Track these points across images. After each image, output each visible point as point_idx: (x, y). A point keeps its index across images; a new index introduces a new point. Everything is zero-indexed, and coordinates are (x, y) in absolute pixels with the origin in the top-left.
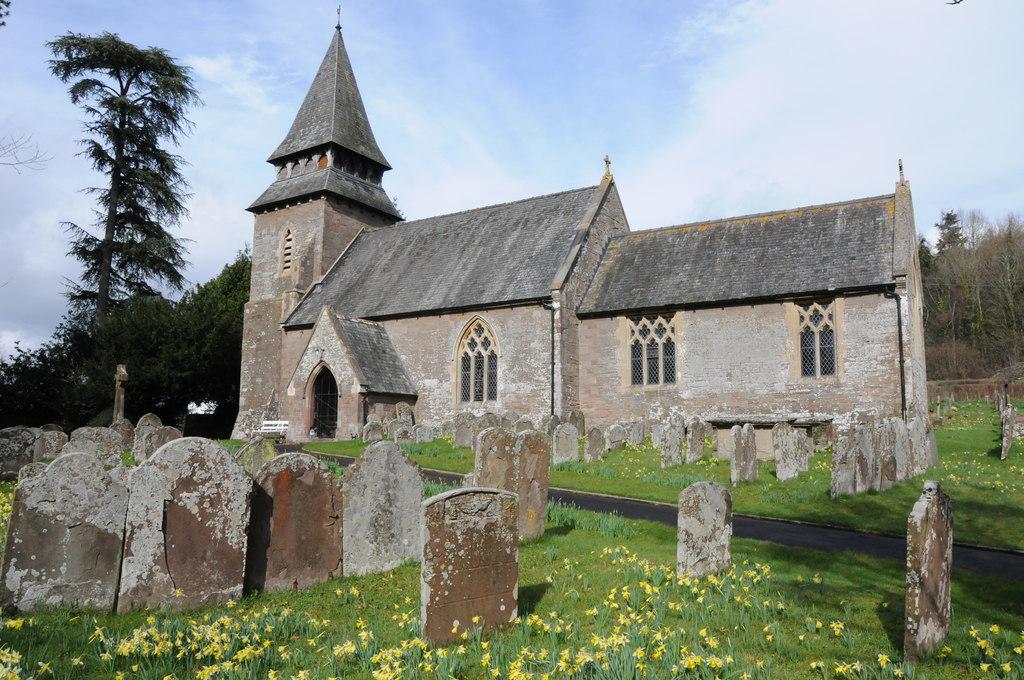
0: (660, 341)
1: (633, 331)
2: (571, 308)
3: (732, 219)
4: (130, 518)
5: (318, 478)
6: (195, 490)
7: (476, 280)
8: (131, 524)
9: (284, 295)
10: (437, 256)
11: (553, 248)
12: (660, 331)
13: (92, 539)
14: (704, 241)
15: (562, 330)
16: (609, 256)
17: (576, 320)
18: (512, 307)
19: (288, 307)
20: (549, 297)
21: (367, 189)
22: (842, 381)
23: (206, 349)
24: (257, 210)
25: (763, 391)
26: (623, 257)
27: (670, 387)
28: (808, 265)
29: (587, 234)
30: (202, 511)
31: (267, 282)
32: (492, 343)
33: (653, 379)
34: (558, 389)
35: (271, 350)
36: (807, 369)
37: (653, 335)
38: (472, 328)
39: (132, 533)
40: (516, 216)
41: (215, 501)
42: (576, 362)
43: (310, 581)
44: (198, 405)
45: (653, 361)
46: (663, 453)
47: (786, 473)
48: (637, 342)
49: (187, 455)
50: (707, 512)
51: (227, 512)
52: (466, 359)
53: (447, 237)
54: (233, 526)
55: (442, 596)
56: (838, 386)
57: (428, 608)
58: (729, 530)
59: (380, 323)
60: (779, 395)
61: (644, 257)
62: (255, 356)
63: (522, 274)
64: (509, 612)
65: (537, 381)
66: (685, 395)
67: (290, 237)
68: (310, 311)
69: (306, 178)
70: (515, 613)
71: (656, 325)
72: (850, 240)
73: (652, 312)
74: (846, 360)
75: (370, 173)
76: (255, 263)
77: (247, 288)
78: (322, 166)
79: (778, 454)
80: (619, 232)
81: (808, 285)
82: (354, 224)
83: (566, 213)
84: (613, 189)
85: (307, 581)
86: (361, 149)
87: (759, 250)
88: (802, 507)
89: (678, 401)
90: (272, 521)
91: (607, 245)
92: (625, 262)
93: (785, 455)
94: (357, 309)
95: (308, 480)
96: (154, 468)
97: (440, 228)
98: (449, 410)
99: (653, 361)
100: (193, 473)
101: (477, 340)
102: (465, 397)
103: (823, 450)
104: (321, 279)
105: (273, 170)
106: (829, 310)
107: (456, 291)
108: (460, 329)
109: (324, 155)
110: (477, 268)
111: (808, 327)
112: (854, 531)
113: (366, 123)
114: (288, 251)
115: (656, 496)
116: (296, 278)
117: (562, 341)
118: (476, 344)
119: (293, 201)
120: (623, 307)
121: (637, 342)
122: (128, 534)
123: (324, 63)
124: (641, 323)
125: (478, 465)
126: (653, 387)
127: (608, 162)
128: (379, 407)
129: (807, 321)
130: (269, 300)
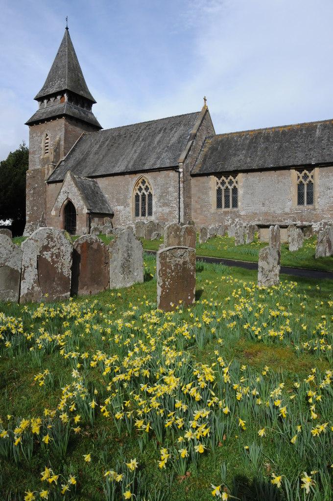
0: (231, 188)
1: (218, 183)
2: (188, 172)
3: (266, 129)
4: (23, 263)
5: (99, 246)
6: (50, 251)
7: (141, 157)
8: (24, 266)
9: (46, 166)
10: (121, 146)
11: (179, 142)
12: (231, 183)
13: (8, 272)
14: (252, 139)
15: (184, 182)
16: (205, 146)
17: (190, 178)
18: (159, 171)
19: (48, 173)
20: (178, 166)
21: (84, 113)
22: (317, 207)
23: (9, 193)
24: (30, 124)
25: (279, 212)
26: (213, 147)
27: (235, 209)
28: (302, 151)
29: (195, 135)
30: (53, 260)
31: (37, 160)
32: (150, 189)
33: (227, 206)
34: (182, 210)
35: (41, 194)
36: (300, 202)
37: (227, 184)
38: (140, 181)
39: (25, 270)
40: (160, 127)
41: (58, 256)
42: (190, 198)
43: (96, 291)
44: (5, 221)
45: (227, 197)
46: (236, 239)
47: (293, 248)
48: (219, 188)
49: (46, 235)
50: (270, 259)
51: (63, 261)
52: (137, 196)
53: (126, 137)
54: (65, 266)
55: (166, 292)
56: (315, 209)
57: (160, 297)
58: (279, 267)
59: (94, 179)
60: (287, 214)
61: (223, 147)
62: (33, 196)
63: (164, 154)
64: (192, 300)
65: (172, 207)
66: (242, 213)
67: (47, 137)
68: (59, 174)
69: (55, 107)
70: (194, 300)
71: (228, 180)
72: (323, 140)
73: (227, 174)
74: (319, 198)
75: (86, 105)
76: (31, 151)
77: (28, 164)
78: (62, 101)
79: (290, 239)
80: (210, 135)
81: (302, 161)
82: (79, 131)
83: (185, 125)
84: (207, 114)
85: (95, 291)
86: (81, 93)
87: (279, 144)
88: (302, 263)
89: (239, 216)
90: (80, 264)
91: (205, 141)
92: (213, 149)
93: (293, 240)
94: (83, 173)
95: (95, 246)
96: (32, 241)
97: (122, 132)
98: (129, 220)
99: (227, 197)
100: (49, 243)
101: (143, 187)
102: (137, 214)
103: (307, 239)
104: (64, 158)
105: (37, 103)
106: (311, 174)
107: (132, 163)
108: (134, 182)
109: (63, 96)
110: (141, 152)
111: (301, 182)
112: (326, 272)
113: (83, 79)
114: (47, 145)
115: (235, 258)
116: (52, 158)
117: (184, 188)
118: (142, 189)
119: (48, 120)
120: (213, 171)
121: (219, 188)
122: (23, 270)
123: (60, 48)
124: (221, 179)
125: (165, 240)
126: (227, 209)
127: (205, 100)
128: (96, 219)
129: (301, 179)
130: (38, 169)
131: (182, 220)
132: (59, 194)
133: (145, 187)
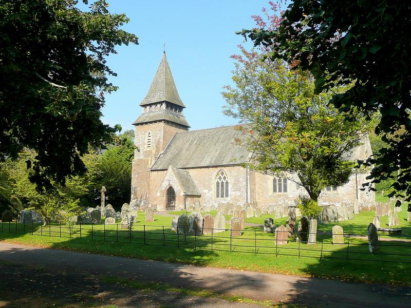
0: (224, 182)
19: (151, 162)
27: (285, 193)
34: (249, 194)
42: (255, 185)
45: (280, 185)
52: (218, 183)
53: (209, 138)
82: (174, 130)
89: (288, 198)
95: (209, 218)
99: (280, 185)
102: (218, 196)
108: (215, 173)
116: (154, 151)
126: (280, 193)
131: (249, 202)
132: (163, 181)
133: (223, 177)
